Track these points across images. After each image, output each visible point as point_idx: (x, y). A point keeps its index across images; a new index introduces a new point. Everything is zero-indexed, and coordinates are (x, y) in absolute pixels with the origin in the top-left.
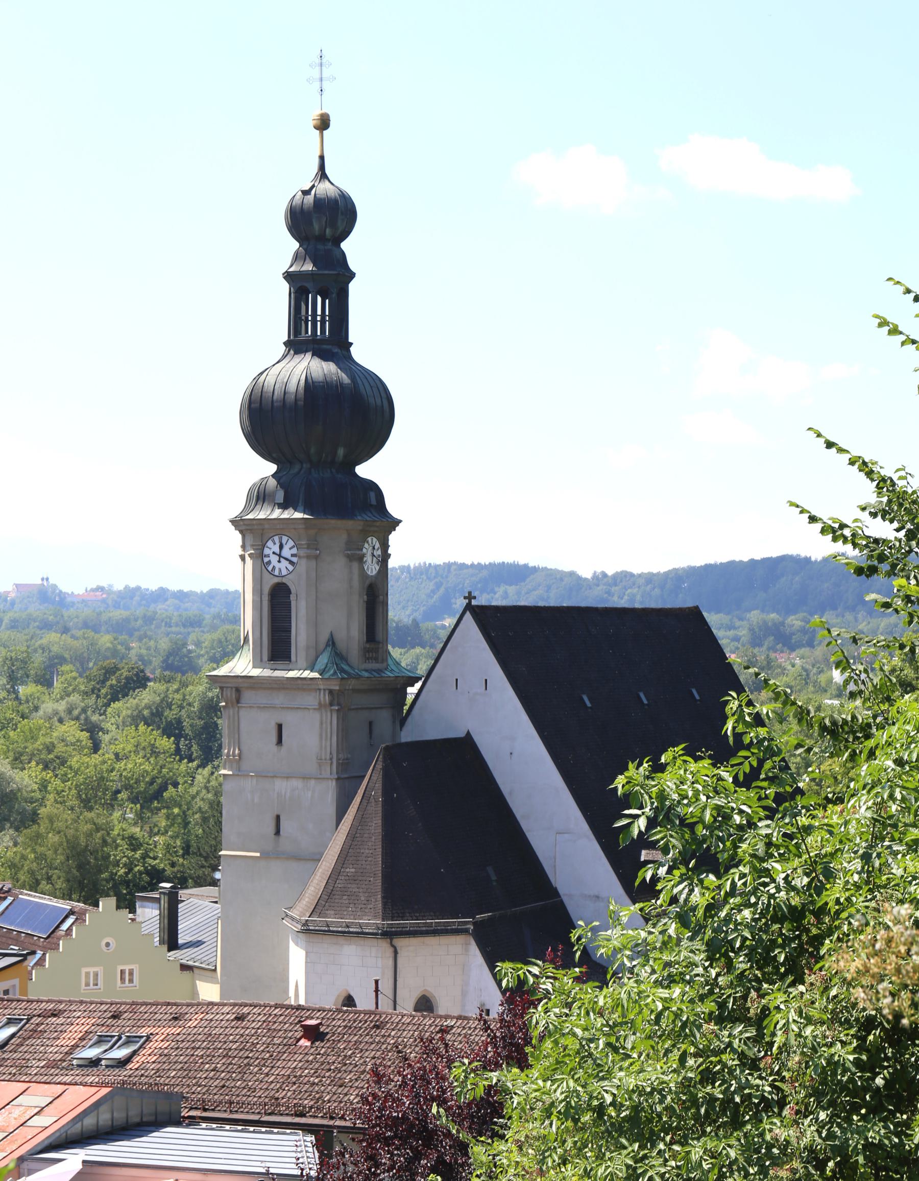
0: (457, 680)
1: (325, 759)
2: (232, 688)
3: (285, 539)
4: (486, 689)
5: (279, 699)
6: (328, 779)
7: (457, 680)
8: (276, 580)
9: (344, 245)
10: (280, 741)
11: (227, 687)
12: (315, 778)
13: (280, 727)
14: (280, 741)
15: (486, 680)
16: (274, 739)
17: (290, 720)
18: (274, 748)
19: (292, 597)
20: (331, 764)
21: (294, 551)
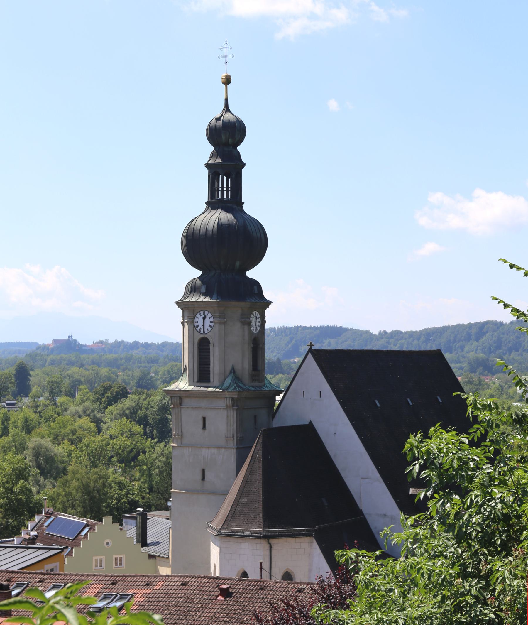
0: (304, 392)
1: (230, 437)
2: (177, 397)
3: (206, 313)
4: (320, 397)
5: (204, 403)
6: (231, 448)
7: (304, 392)
8: (202, 336)
9: (239, 148)
10: (204, 427)
11: (174, 397)
12: (225, 448)
13: (204, 419)
14: (204, 427)
15: (320, 392)
16: (201, 425)
17: (210, 415)
18: (201, 431)
19: (211, 346)
20: (233, 440)
21: (212, 319)
